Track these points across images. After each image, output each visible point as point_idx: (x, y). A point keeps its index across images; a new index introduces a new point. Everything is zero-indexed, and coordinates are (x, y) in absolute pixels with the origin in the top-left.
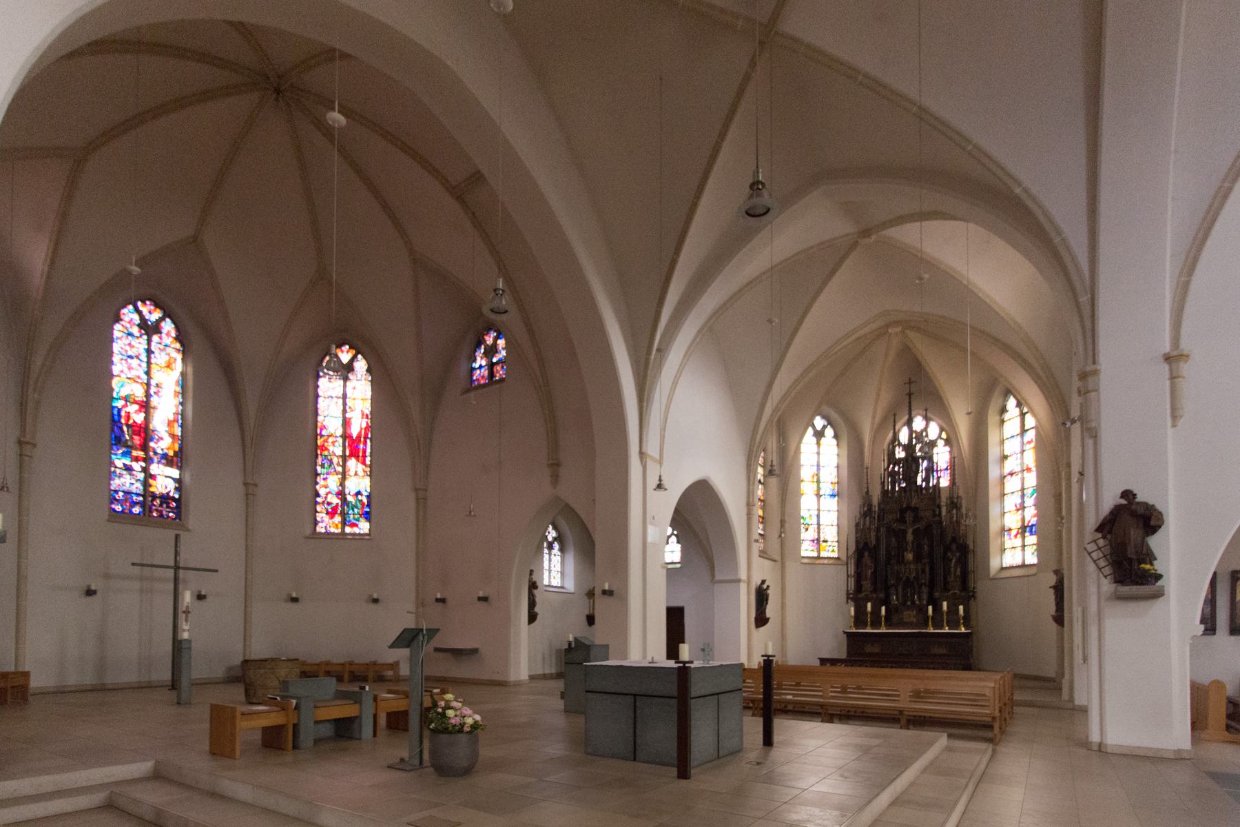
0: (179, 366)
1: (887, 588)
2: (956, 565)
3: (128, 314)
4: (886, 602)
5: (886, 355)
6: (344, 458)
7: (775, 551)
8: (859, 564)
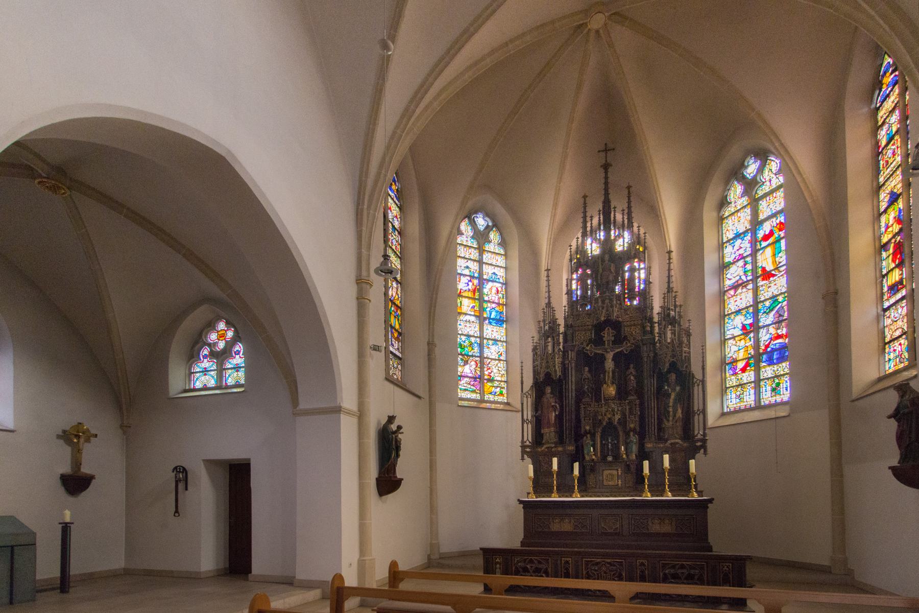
1: (578, 436)
2: (675, 403)
4: (578, 455)
5: (579, 87)
7: (419, 384)
8: (538, 405)
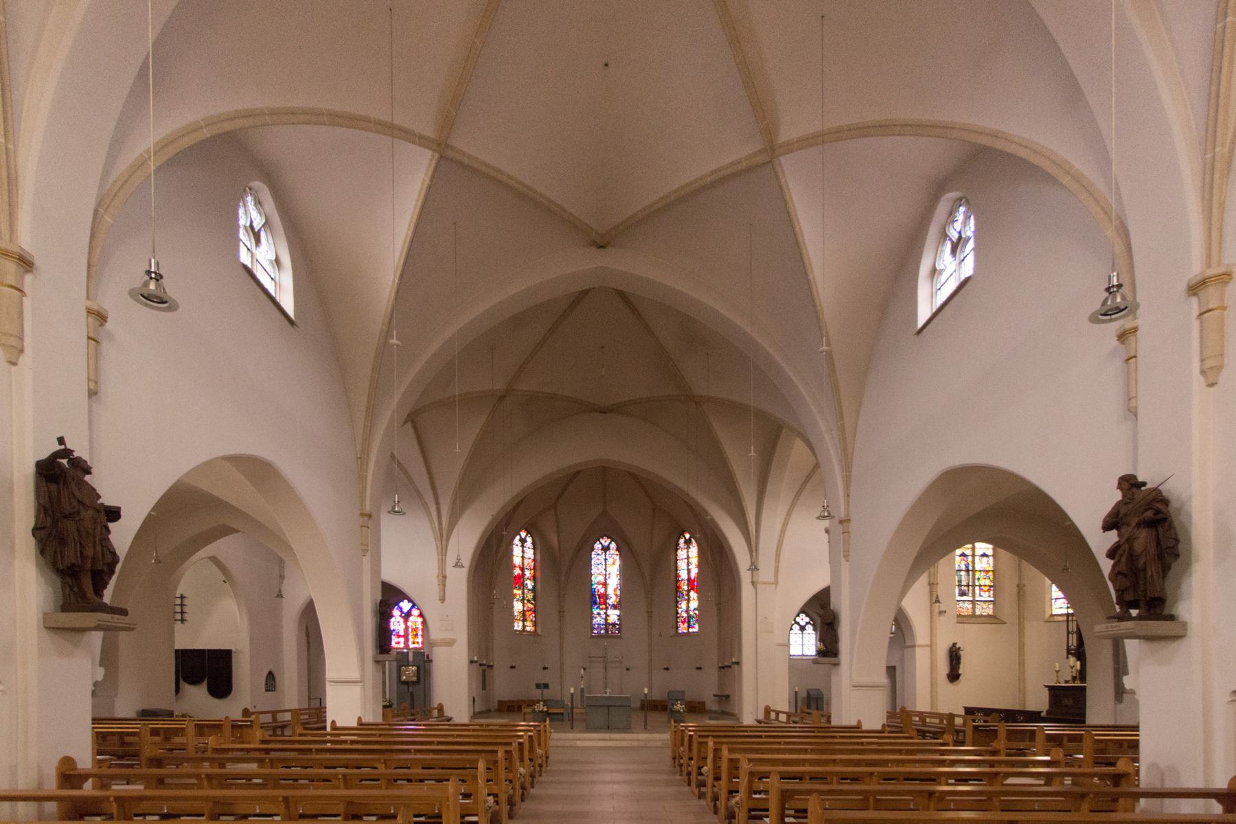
0: (618, 562)
3: (598, 546)
6: (689, 591)
